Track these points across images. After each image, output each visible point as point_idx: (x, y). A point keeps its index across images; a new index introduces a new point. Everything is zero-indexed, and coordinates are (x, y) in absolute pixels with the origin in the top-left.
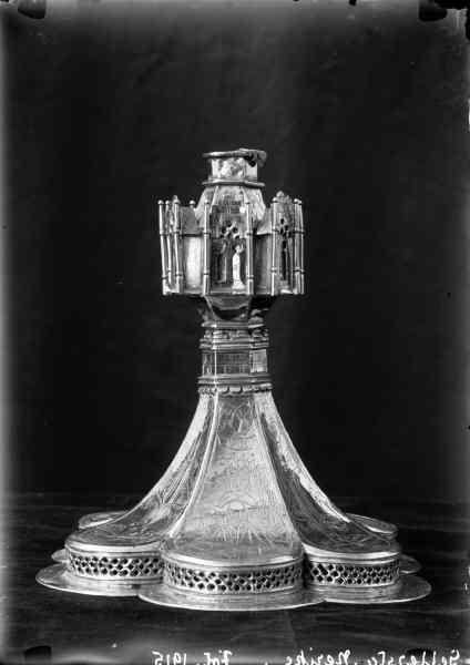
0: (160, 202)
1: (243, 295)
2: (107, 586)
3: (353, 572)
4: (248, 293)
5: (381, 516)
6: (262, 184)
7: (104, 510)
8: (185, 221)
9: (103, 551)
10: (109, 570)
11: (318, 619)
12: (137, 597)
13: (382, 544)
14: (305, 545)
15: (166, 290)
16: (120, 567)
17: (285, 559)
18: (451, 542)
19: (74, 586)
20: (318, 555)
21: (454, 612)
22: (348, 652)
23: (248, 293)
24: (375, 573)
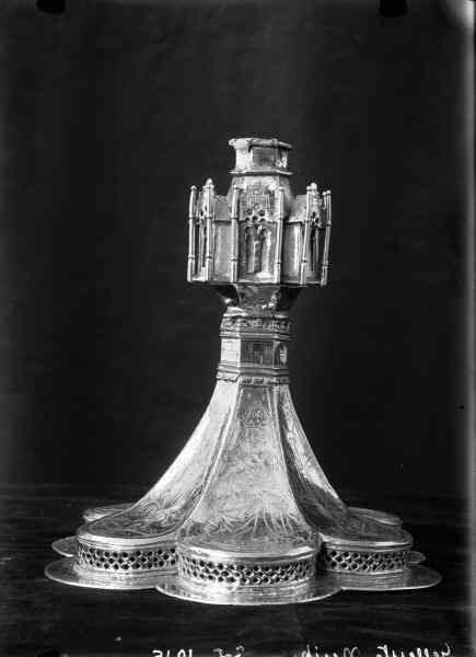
0: (193, 187)
1: (270, 284)
2: (113, 580)
3: (364, 559)
4: (276, 280)
5: (389, 511)
6: (289, 174)
7: (388, 511)
8: (217, 209)
9: (117, 545)
10: (120, 565)
11: (326, 613)
12: (154, 589)
13: (384, 533)
14: (321, 535)
15: (189, 279)
16: (121, 561)
17: (304, 550)
18: (458, 537)
19: (93, 582)
20: (335, 543)
21: (462, 609)
22: (231, 142)
23: (275, 281)
24: (386, 560)
